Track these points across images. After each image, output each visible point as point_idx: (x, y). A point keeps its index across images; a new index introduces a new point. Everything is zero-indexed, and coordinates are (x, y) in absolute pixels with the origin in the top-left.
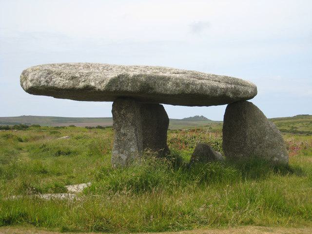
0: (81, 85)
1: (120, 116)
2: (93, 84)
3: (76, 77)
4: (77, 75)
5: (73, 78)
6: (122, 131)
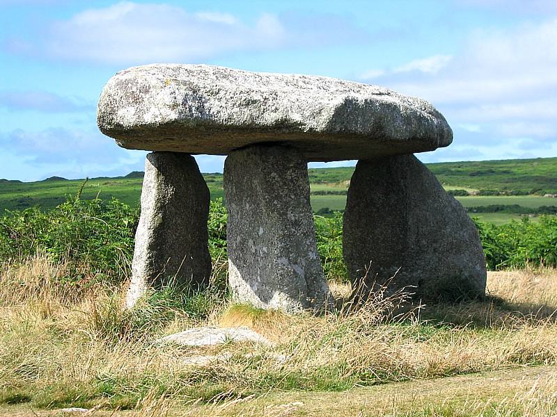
0: (270, 118)
1: (285, 184)
2: (296, 117)
3: (254, 102)
4: (256, 97)
5: (249, 103)
6: (291, 216)
